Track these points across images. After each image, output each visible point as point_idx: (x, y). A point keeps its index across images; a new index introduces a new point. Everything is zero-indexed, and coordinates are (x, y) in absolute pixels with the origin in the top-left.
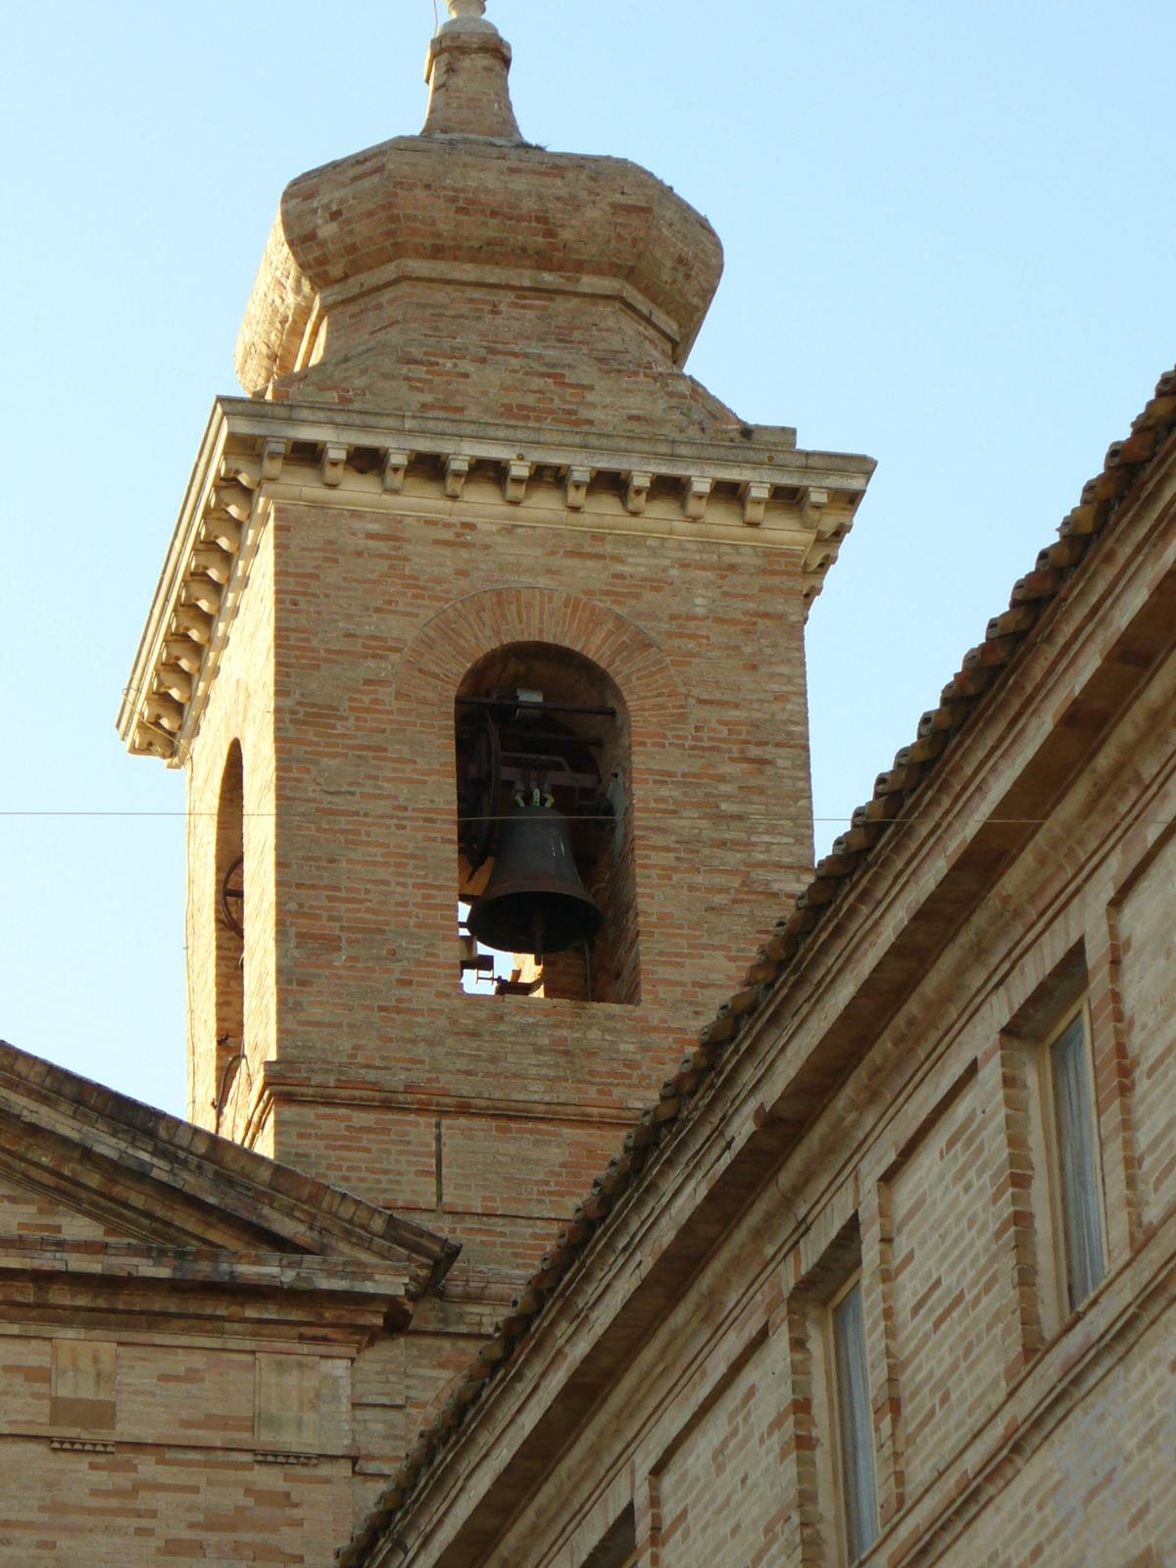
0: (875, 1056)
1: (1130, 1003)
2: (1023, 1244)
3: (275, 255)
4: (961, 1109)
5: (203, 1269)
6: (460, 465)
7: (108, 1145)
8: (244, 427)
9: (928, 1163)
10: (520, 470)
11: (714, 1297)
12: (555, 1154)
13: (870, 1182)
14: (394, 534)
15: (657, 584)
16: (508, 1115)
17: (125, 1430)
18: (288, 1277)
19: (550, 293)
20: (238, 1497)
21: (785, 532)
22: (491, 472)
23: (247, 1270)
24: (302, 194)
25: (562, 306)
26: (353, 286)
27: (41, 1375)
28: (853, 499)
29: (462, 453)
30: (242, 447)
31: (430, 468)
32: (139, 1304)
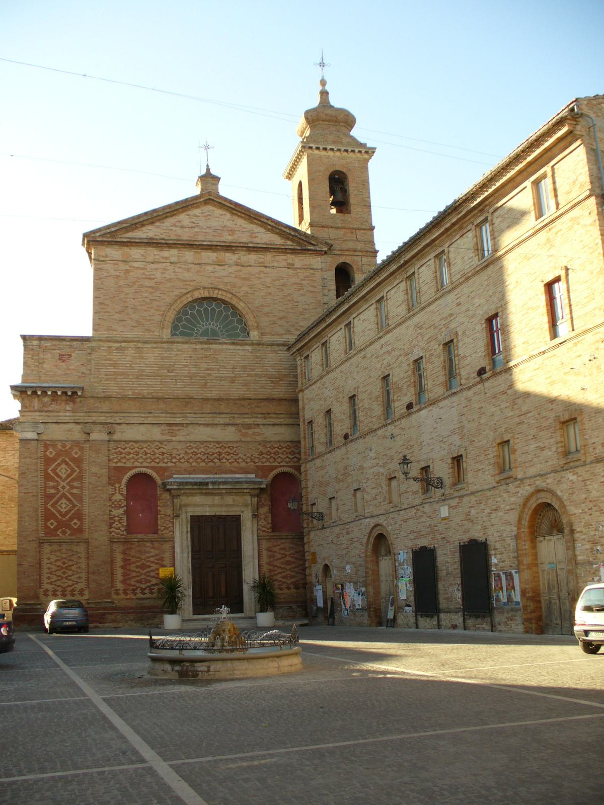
0: (418, 256)
1: (450, 257)
2: (436, 279)
3: (302, 121)
4: (428, 263)
5: (304, 248)
6: (328, 149)
7: (293, 233)
8: (304, 145)
9: (423, 268)
10: (336, 149)
11: (396, 276)
12: (342, 232)
13: (416, 268)
14: (320, 157)
15: (351, 163)
16: (337, 228)
17: (295, 266)
18: (314, 248)
19: (336, 125)
20: (309, 274)
21: (366, 156)
22: (332, 150)
23: (309, 248)
24: (307, 113)
25: (338, 127)
26: (313, 125)
27: (285, 260)
28: (374, 152)
29: (329, 147)
30: (303, 147)
31: (325, 149)
32: (297, 251)
